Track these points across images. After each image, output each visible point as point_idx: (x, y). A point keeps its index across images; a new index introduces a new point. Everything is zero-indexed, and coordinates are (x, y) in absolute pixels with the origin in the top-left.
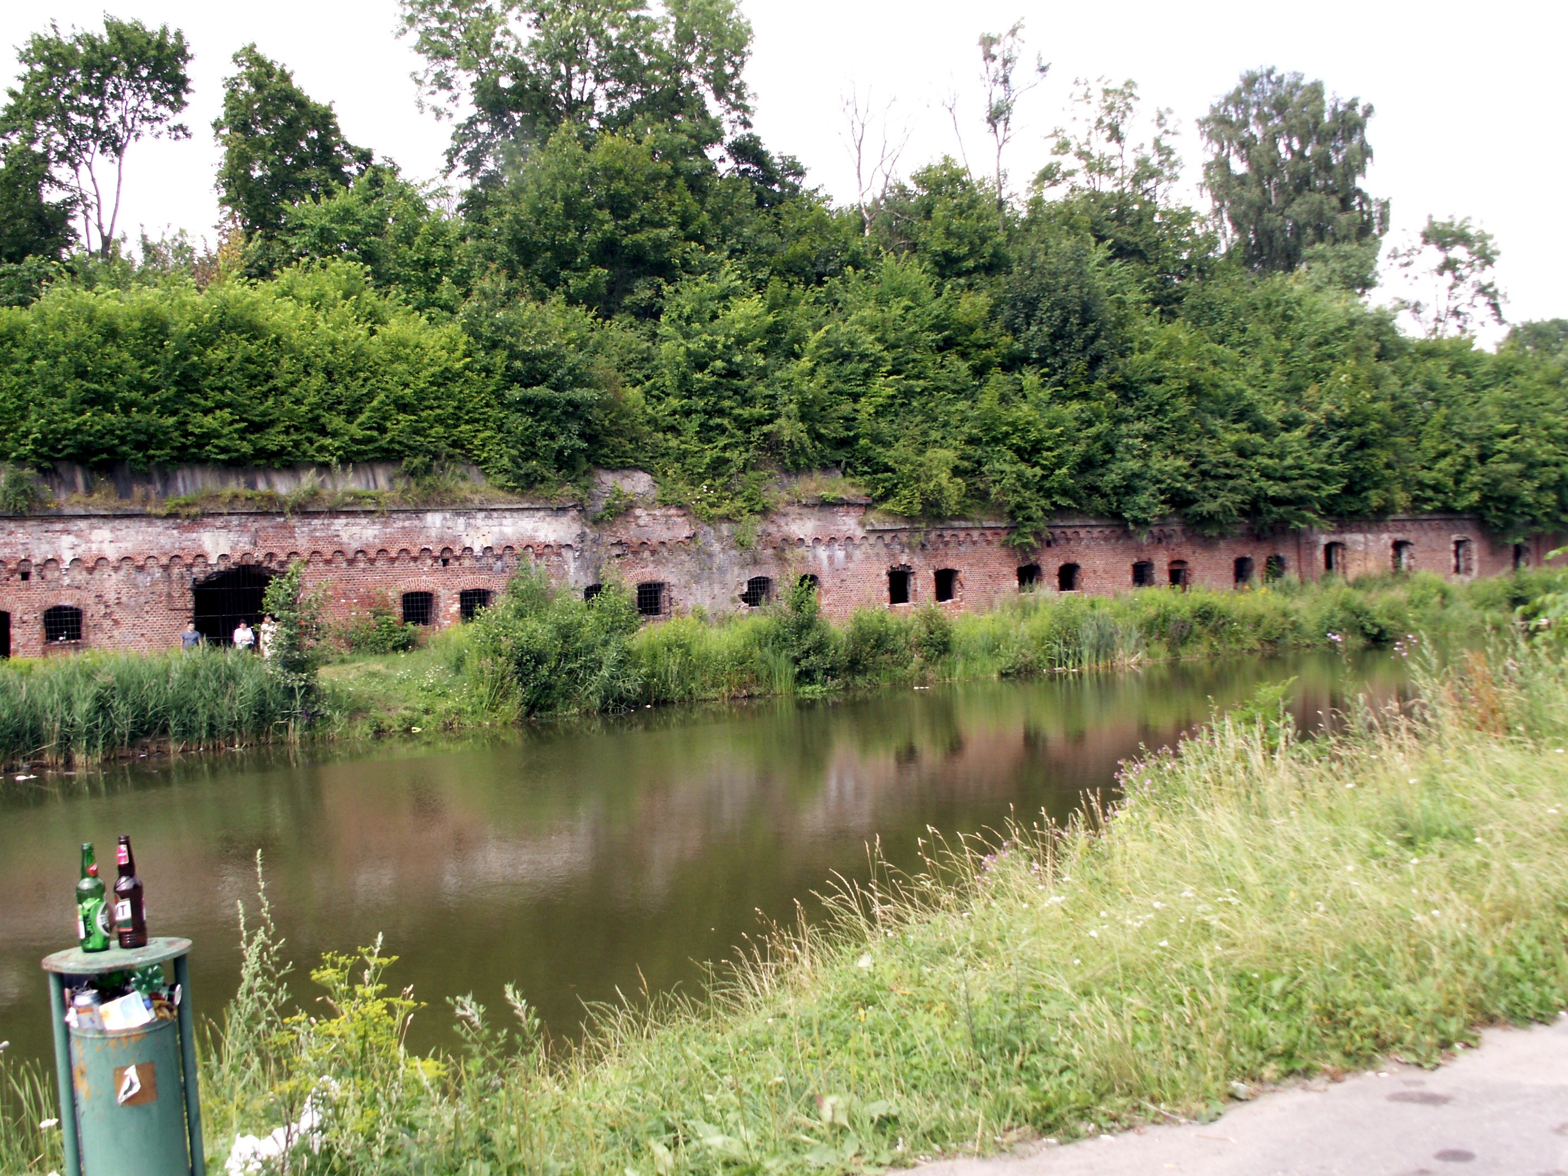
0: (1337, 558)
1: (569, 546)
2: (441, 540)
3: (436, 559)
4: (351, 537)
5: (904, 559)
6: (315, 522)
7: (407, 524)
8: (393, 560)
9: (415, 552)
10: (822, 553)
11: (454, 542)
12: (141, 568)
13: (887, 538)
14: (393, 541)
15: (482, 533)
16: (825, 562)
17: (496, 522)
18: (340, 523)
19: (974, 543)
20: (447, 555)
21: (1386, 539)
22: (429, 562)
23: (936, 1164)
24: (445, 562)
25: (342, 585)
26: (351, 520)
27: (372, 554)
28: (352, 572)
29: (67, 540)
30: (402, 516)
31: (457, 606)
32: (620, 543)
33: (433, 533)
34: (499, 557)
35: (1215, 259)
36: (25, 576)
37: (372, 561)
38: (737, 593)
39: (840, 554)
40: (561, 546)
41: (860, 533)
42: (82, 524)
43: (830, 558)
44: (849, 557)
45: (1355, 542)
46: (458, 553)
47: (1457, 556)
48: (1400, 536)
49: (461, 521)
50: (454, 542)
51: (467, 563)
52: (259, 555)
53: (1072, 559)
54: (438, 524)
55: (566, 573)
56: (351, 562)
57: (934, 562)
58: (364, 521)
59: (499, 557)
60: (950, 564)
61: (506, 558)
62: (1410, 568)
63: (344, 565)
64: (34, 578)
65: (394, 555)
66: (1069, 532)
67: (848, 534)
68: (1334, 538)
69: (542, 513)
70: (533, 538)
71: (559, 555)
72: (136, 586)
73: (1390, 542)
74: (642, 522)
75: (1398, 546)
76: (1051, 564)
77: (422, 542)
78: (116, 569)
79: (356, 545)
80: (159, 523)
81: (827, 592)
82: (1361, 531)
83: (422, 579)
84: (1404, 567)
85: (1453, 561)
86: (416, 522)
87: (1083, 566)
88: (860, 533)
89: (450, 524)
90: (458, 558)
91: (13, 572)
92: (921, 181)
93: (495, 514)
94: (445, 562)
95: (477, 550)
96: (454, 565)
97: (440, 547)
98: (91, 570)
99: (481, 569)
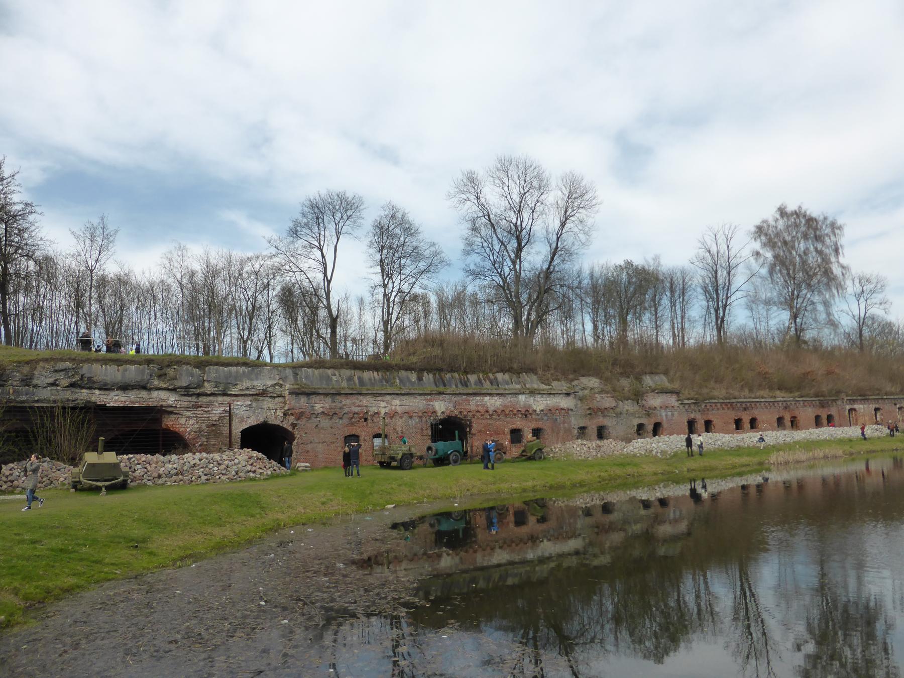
2: (525, 407)
5: (692, 416)
6: (478, 398)
9: (335, 417)
12: (411, 417)
13: (687, 407)
15: (540, 404)
16: (664, 418)
18: (487, 399)
21: (873, 406)
23: (896, 640)
27: (420, 414)
29: (383, 404)
33: (522, 404)
34: (546, 414)
36: (366, 420)
39: (670, 413)
42: (388, 398)
43: (666, 415)
44: (673, 415)
48: (877, 406)
52: (457, 412)
59: (546, 414)
60: (711, 417)
64: (369, 421)
68: (851, 407)
72: (408, 425)
75: (876, 410)
76: (746, 420)
78: (401, 417)
80: (418, 397)
83: (518, 424)
91: (361, 418)
94: (526, 416)
95: (538, 410)
98: (391, 418)
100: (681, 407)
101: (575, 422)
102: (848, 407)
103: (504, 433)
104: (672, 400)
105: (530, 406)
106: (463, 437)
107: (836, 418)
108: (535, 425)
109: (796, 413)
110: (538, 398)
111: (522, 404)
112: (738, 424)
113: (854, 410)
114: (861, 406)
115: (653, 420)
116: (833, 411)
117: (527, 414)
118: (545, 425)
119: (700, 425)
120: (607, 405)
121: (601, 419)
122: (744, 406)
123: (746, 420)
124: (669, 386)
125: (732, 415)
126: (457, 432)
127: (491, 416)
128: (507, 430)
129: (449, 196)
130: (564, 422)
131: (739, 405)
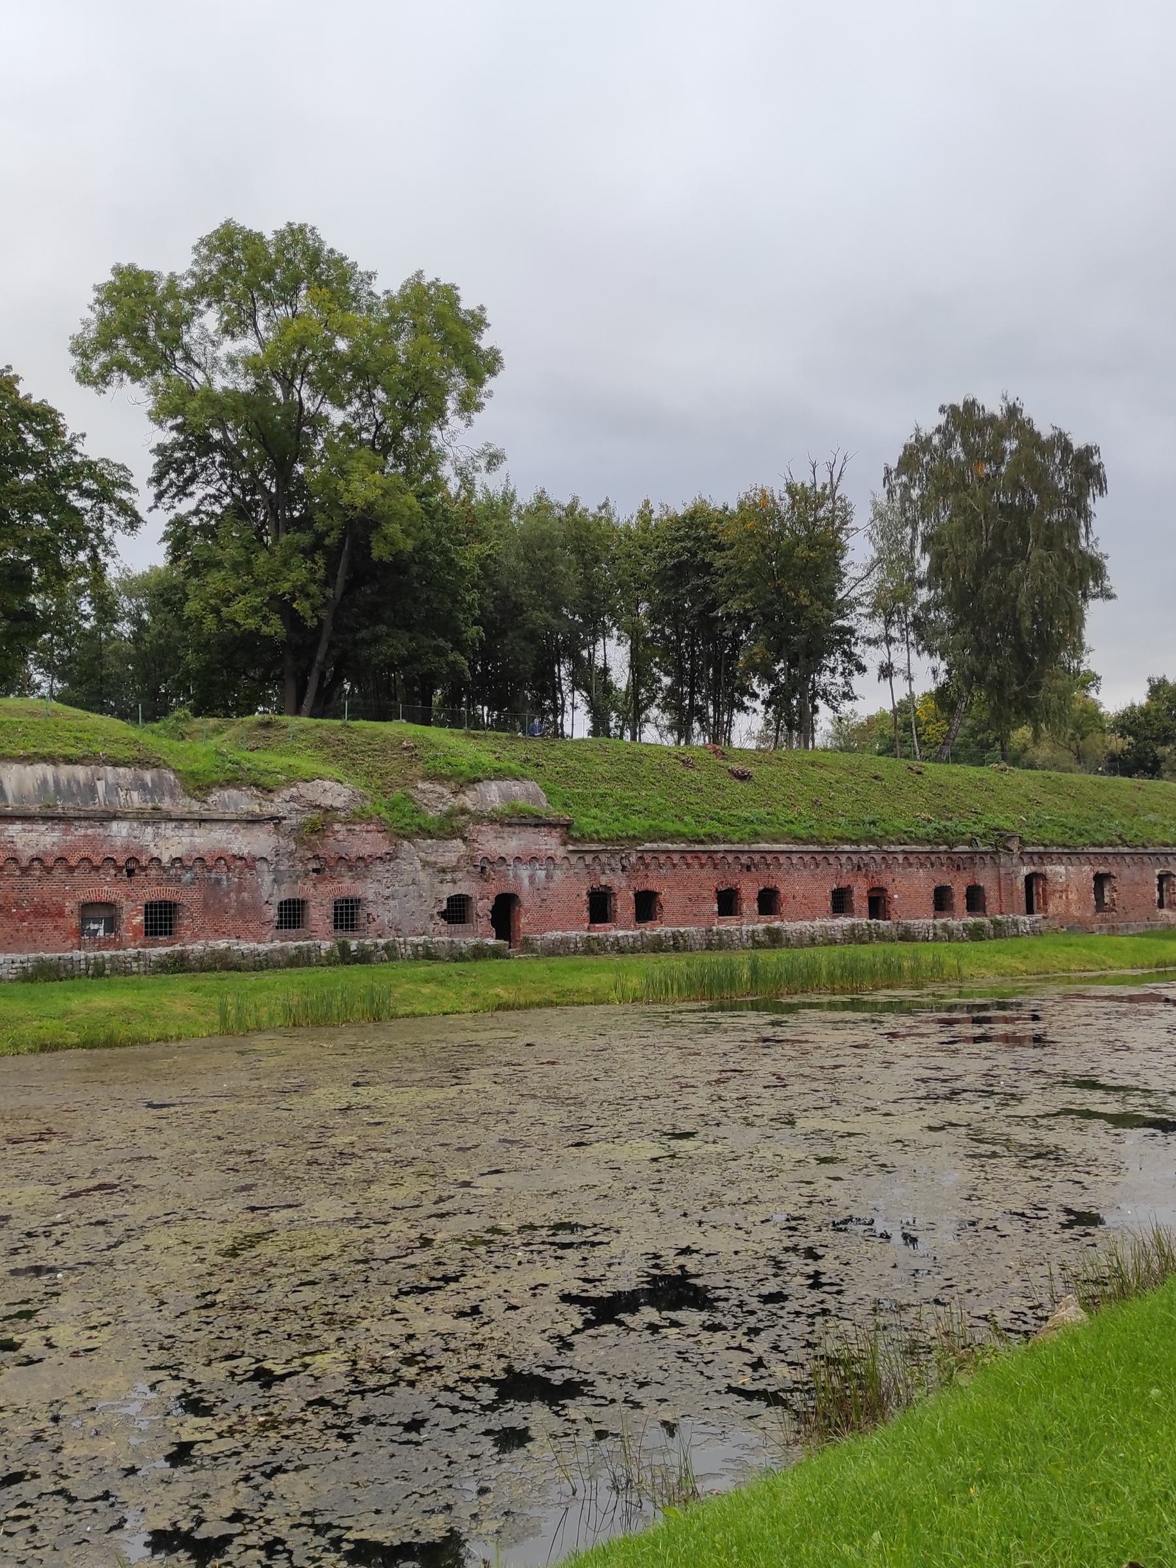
0: (1038, 889)
1: (265, 859)
2: (127, 849)
3: (119, 869)
4: (26, 844)
7: (90, 832)
8: (71, 869)
10: (524, 872)
11: (141, 852)
13: (589, 859)
14: (74, 848)
16: (526, 881)
17: (187, 832)
18: (15, 829)
19: (674, 866)
20: (132, 865)
22: (113, 872)
24: (130, 873)
25: (14, 895)
26: (28, 827)
28: (27, 881)
30: (86, 824)
31: (139, 919)
32: (316, 857)
33: (118, 842)
35: (24, 662)
37: (49, 870)
38: (436, 910)
39: (541, 874)
40: (255, 859)
41: (561, 852)
43: (532, 878)
44: (549, 877)
45: (1056, 874)
46: (144, 863)
47: (1160, 889)
48: (1102, 869)
49: (149, 830)
50: (141, 852)
51: (153, 873)
53: (772, 884)
54: (124, 833)
55: (259, 887)
56: (25, 871)
57: (634, 883)
58: (43, 828)
60: (652, 885)
61: (197, 870)
62: (1113, 900)
63: (18, 873)
65: (73, 863)
66: (769, 858)
67: (550, 853)
69: (236, 825)
70: (224, 850)
71: (253, 868)
73: (1092, 875)
74: (341, 838)
75: (1100, 880)
76: (749, 891)
77: (105, 851)
79: (31, 852)
81: (527, 911)
82: (519, 920)
83: (107, 888)
84: (1107, 900)
85: (1157, 895)
86: (101, 830)
87: (782, 891)
88: (561, 852)
89: (136, 833)
90: (144, 869)
92: (1100, 466)
93: (186, 825)
94: (130, 873)
95: (165, 859)
96: (140, 877)
97: (126, 856)
99: (169, 880)
100: (574, 859)
101: (271, 892)
102: (1025, 871)
103: (61, 914)
104: (549, 843)
105: (143, 849)
106: (185, 1395)
107: (991, 894)
108: (154, 893)
109: (885, 880)
110: (168, 829)
111: (118, 842)
112: (728, 903)
113: (1043, 876)
114: (1061, 869)
115: (494, 888)
116: (986, 879)
117: (131, 867)
118: (188, 897)
119: (624, 905)
120: (366, 851)
121: (347, 882)
122: (744, 859)
123: (749, 891)
124: (543, 806)
125: (709, 881)
126: (20, 425)
127: (25, 871)
128: (70, 905)
129: (97, 289)
130: (240, 888)
131: (730, 858)
